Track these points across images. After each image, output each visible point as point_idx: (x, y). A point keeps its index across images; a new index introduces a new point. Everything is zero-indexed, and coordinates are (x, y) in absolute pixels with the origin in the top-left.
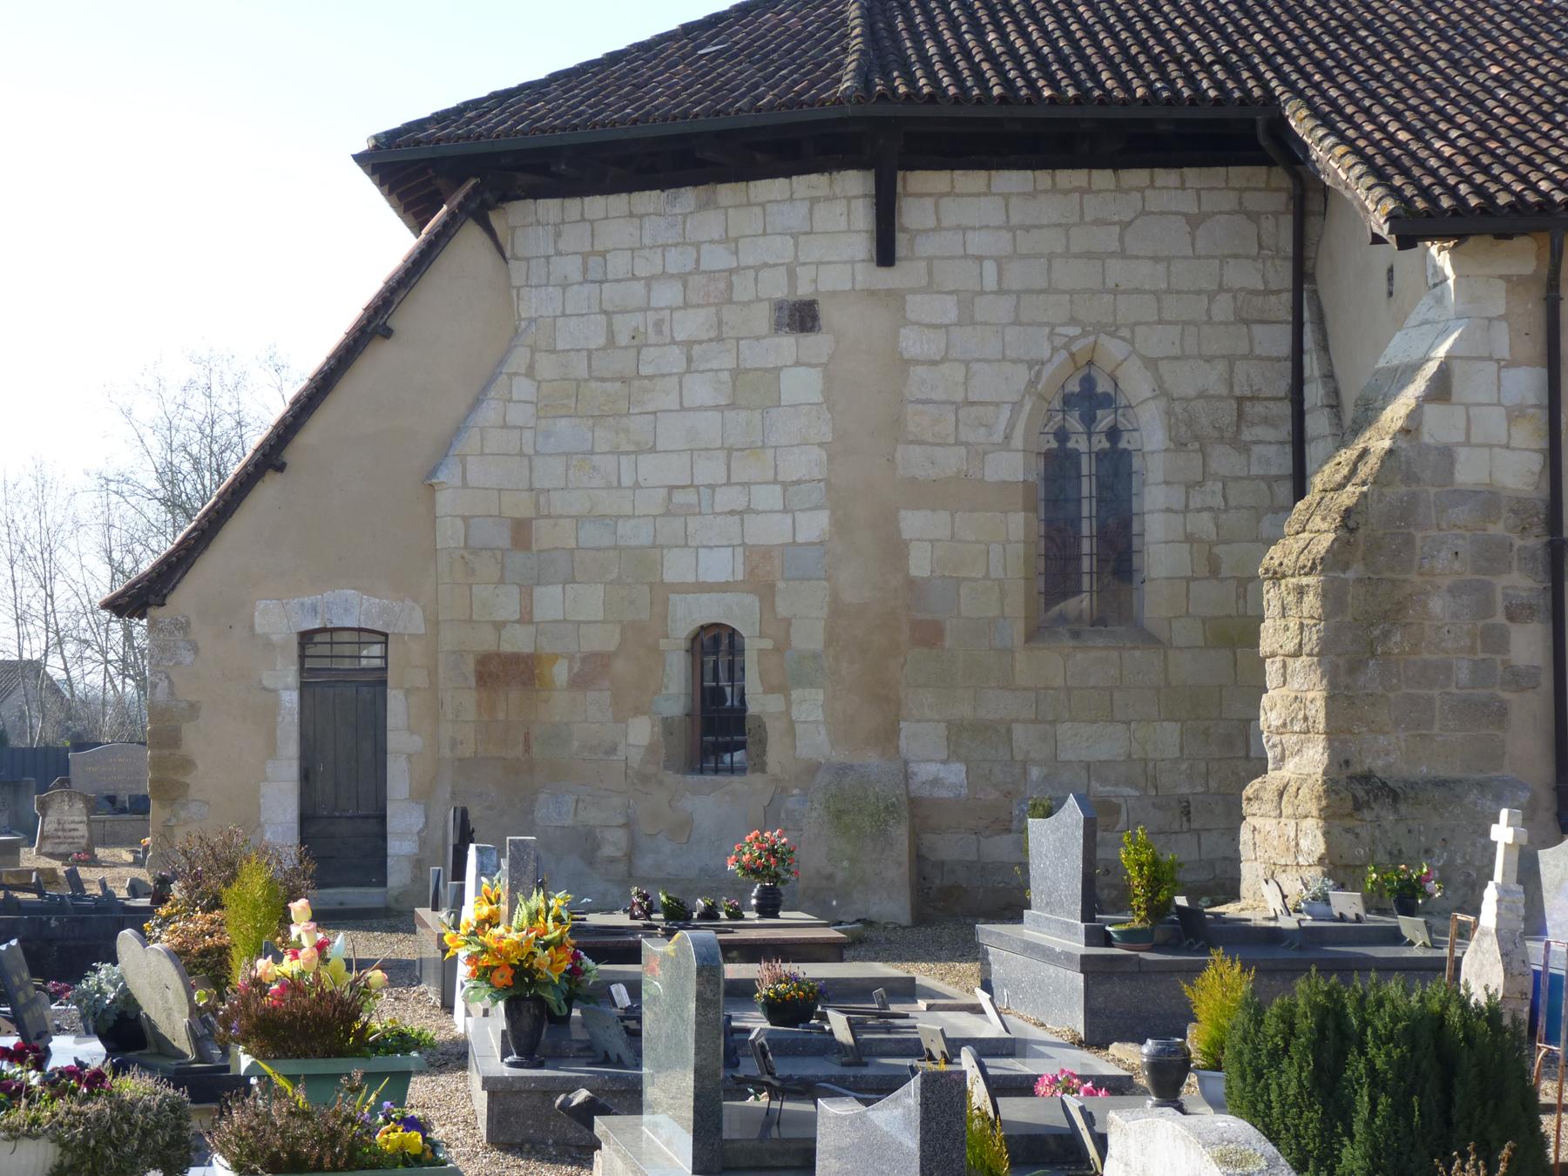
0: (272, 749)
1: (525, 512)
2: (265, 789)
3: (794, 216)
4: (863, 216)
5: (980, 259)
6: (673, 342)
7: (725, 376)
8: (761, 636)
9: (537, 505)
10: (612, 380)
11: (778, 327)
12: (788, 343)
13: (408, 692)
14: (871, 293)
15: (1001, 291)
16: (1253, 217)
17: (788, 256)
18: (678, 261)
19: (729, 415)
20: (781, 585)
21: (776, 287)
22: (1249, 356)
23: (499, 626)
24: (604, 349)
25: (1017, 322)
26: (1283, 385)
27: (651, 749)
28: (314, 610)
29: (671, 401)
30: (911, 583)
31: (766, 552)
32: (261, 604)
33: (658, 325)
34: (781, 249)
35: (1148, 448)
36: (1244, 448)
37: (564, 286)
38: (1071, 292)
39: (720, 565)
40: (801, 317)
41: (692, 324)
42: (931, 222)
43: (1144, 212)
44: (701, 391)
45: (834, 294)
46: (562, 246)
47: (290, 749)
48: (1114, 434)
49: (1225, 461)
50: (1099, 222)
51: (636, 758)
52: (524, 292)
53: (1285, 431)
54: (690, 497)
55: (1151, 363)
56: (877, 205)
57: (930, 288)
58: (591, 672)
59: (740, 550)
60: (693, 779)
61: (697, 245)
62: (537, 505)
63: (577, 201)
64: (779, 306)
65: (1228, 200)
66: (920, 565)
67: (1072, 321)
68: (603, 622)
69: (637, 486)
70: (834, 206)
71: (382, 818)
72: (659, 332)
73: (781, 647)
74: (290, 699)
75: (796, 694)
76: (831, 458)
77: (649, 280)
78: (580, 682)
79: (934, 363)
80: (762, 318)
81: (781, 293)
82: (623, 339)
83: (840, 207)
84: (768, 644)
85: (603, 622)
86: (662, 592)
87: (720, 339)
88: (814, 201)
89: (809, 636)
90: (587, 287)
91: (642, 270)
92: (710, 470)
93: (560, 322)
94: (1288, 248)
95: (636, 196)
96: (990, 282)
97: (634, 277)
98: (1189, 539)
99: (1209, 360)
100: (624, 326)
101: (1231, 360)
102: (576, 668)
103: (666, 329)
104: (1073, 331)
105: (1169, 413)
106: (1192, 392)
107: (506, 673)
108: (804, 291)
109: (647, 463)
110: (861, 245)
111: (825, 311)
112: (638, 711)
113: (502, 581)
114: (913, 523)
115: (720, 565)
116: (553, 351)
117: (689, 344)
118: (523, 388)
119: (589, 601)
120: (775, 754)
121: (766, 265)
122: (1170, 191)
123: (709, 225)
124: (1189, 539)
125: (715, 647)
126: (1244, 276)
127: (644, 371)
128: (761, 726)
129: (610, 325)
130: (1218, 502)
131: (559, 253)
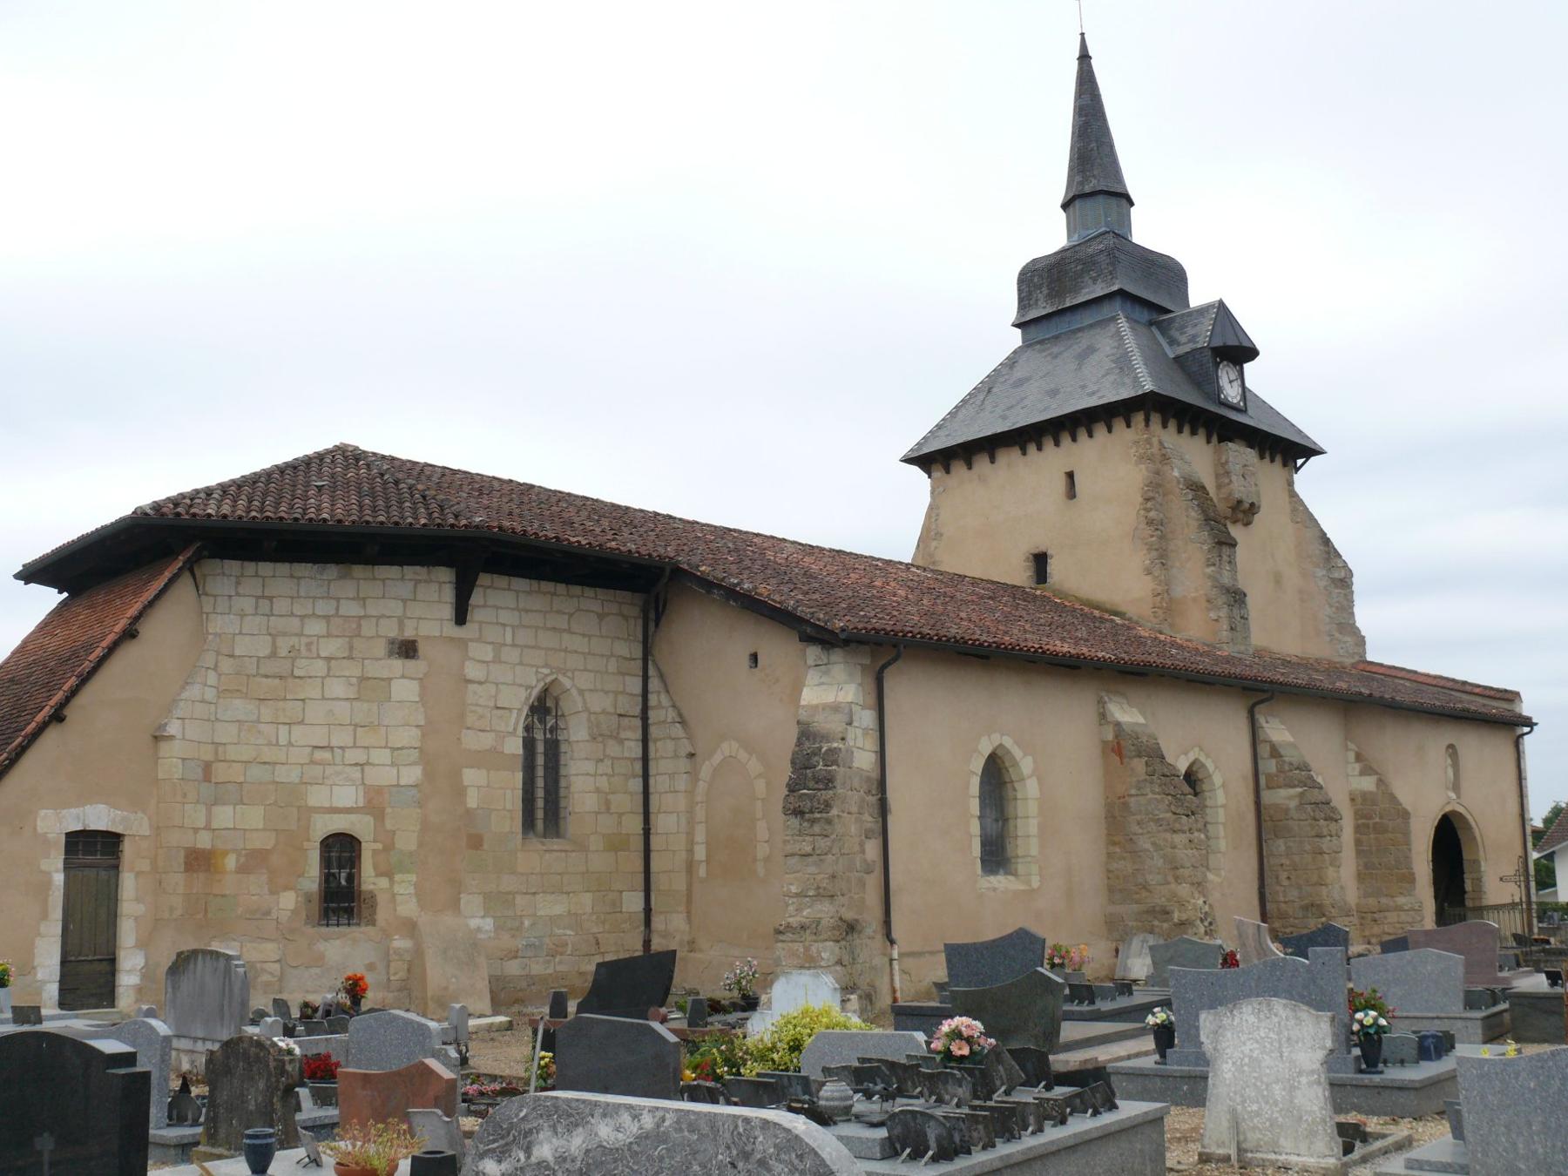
0: (45, 916)
1: (209, 757)
2: (38, 941)
3: (405, 589)
4: (449, 594)
5: (504, 625)
6: (319, 657)
7: (354, 680)
8: (375, 841)
9: (216, 753)
10: (274, 677)
11: (390, 654)
12: (398, 664)
13: (138, 874)
14: (452, 639)
15: (514, 645)
16: (626, 618)
17: (399, 612)
18: (324, 607)
19: (356, 704)
20: (389, 810)
21: (391, 630)
22: (623, 693)
23: (196, 830)
24: (269, 657)
25: (521, 663)
26: (637, 710)
27: (295, 912)
28: (78, 818)
29: (316, 693)
30: (468, 811)
31: (379, 790)
32: (42, 813)
33: (309, 645)
34: (395, 608)
35: (573, 738)
36: (621, 742)
37: (242, 615)
38: (548, 649)
39: (347, 796)
40: (407, 649)
41: (331, 647)
42: (481, 602)
43: (579, 610)
44: (337, 688)
45: (428, 637)
46: (241, 591)
47: (57, 914)
48: (554, 729)
49: (613, 749)
50: (558, 612)
51: (284, 917)
52: (212, 616)
53: (639, 734)
54: (327, 755)
55: (581, 692)
56: (457, 589)
57: (480, 640)
58: (254, 861)
59: (361, 788)
60: (324, 930)
61: (338, 600)
62: (216, 753)
63: (253, 564)
64: (392, 642)
65: (614, 608)
66: (472, 801)
67: (546, 666)
68: (264, 830)
69: (290, 744)
70: (437, 587)
71: (113, 961)
72: (309, 650)
73: (389, 848)
74: (59, 878)
75: (397, 877)
76: (423, 735)
77: (302, 617)
78: (243, 869)
79: (480, 683)
80: (380, 648)
81: (393, 634)
82: (283, 652)
83: (435, 587)
84: (379, 846)
85: (264, 830)
86: (307, 812)
87: (350, 658)
88: (417, 582)
89: (407, 841)
90: (258, 619)
91: (298, 610)
92: (341, 738)
93: (237, 638)
94: (640, 637)
95: (296, 565)
96: (509, 640)
97: (292, 615)
98: (598, 790)
99: (606, 693)
100: (283, 645)
101: (616, 693)
102: (242, 860)
103: (314, 648)
104: (546, 671)
105: (589, 720)
106: (598, 710)
107: (199, 861)
108: (409, 634)
109: (297, 731)
110: (448, 611)
111: (422, 647)
112: (286, 888)
113: (198, 802)
114: (471, 776)
115: (347, 796)
116: (232, 656)
117: (328, 659)
118: (212, 678)
119: (254, 817)
120: (382, 915)
121: (383, 616)
122: (591, 601)
123: (346, 588)
124: (598, 790)
125: (341, 851)
126: (622, 649)
127: (297, 672)
128: (373, 896)
129: (274, 643)
130: (610, 771)
131: (238, 594)
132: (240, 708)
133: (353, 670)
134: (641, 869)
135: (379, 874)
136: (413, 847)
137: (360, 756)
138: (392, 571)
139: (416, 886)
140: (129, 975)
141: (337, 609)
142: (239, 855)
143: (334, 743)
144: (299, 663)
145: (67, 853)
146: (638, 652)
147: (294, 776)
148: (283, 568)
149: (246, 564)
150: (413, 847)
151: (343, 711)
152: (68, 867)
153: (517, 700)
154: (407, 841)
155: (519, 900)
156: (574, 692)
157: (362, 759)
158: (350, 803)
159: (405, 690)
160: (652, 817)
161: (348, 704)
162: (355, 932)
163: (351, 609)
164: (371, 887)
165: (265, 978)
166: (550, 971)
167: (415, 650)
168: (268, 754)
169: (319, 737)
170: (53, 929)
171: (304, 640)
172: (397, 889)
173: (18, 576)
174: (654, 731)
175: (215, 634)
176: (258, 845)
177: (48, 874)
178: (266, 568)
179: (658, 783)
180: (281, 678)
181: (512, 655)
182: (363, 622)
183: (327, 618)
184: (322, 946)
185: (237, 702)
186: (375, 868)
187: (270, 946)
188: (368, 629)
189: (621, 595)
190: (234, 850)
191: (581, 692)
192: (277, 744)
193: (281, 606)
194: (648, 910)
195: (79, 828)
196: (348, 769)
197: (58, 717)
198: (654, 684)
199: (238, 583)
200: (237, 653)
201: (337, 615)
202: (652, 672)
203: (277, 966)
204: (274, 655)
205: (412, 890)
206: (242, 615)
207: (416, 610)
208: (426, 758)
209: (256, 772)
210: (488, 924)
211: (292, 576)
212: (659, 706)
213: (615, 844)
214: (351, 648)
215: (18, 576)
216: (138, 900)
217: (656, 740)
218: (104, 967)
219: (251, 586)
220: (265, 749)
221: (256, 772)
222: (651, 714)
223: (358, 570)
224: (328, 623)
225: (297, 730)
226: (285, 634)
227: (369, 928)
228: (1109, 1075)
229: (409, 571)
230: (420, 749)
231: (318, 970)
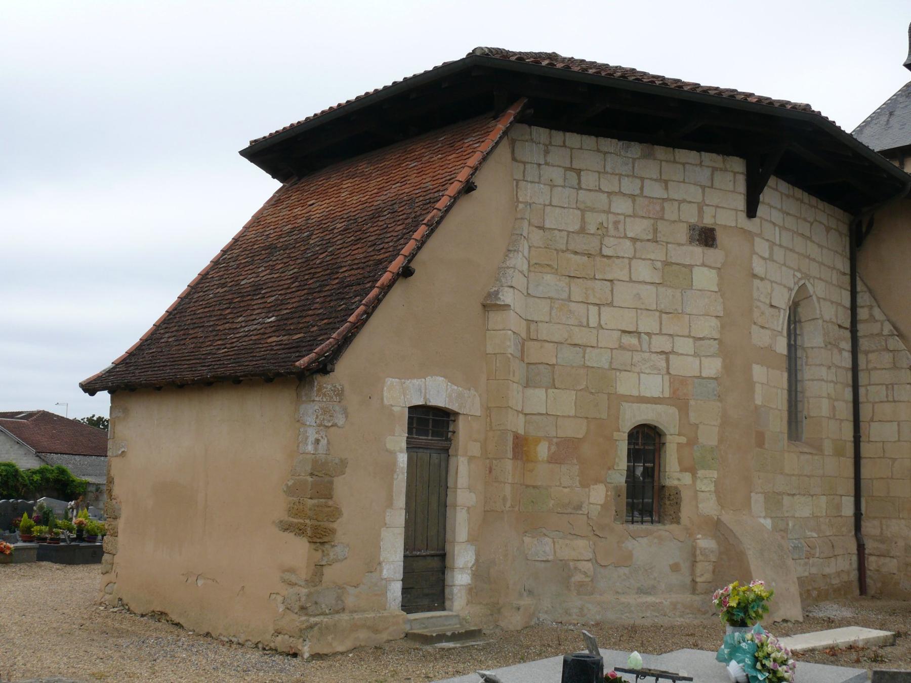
3: (703, 175)
4: (742, 187)
6: (626, 237)
10: (583, 254)
11: (691, 240)
12: (698, 251)
13: (471, 459)
18: (629, 186)
19: (661, 289)
20: (692, 402)
21: (691, 215)
29: (623, 275)
30: (757, 407)
32: (389, 381)
34: (694, 193)
35: (807, 344)
37: (552, 186)
40: (706, 237)
44: (643, 271)
46: (549, 159)
47: (401, 501)
54: (634, 341)
55: (818, 298)
58: (565, 450)
59: (667, 377)
60: (636, 527)
63: (561, 133)
64: (692, 228)
67: (799, 270)
68: (575, 417)
69: (600, 326)
72: (617, 228)
73: (693, 442)
74: (403, 459)
75: (701, 473)
76: (723, 327)
77: (610, 194)
78: (554, 459)
80: (682, 234)
81: (694, 220)
82: (592, 229)
84: (683, 440)
88: (714, 169)
89: (709, 436)
90: (567, 191)
92: (648, 324)
100: (593, 221)
102: (553, 448)
103: (621, 227)
107: (521, 447)
108: (708, 221)
110: (740, 203)
111: (720, 236)
112: (597, 481)
115: (654, 385)
116: (542, 228)
117: (634, 240)
119: (565, 402)
120: (686, 512)
121: (684, 201)
123: (649, 169)
131: (547, 164)
132: (550, 283)
133: (657, 253)
134: (852, 475)
135: (683, 470)
136: (714, 442)
137: (661, 343)
138: (690, 156)
139: (716, 483)
140: (460, 578)
141: (642, 189)
142: (550, 444)
143: (640, 330)
144: (609, 241)
145: (410, 431)
146: (843, 265)
147: (604, 362)
148: (589, 141)
149: (554, 132)
150: (714, 442)
151: (649, 294)
152: (411, 447)
153: (782, 299)
154: (709, 436)
155: (786, 500)
156: (814, 298)
157: (668, 348)
158: (656, 394)
159: (705, 278)
160: (863, 426)
161: (653, 289)
162: (663, 530)
163: (655, 190)
164: (676, 483)
165: (578, 578)
166: (806, 574)
167: (714, 239)
168: (580, 336)
169: (627, 321)
170: (397, 518)
171: (612, 218)
172: (700, 485)
173: (244, 153)
174: (864, 344)
175: (526, 203)
176: (570, 433)
177: (392, 453)
178: (573, 139)
179: (871, 393)
180: (589, 255)
181: (779, 254)
182: (666, 204)
183: (633, 197)
184: (630, 544)
185: (548, 277)
186: (680, 463)
187: (581, 543)
188: (671, 212)
189: (839, 212)
190: (548, 439)
191: (818, 298)
192: (588, 326)
193: (589, 179)
194: (858, 516)
195: (420, 402)
196: (654, 357)
197: (407, 272)
198: (863, 299)
199: (547, 152)
200: (547, 225)
201: (641, 194)
202: (860, 287)
203: (589, 565)
204: (582, 230)
205: (712, 488)
206: (552, 186)
207: (713, 198)
208: (724, 351)
209: (568, 355)
210: (768, 523)
211: (598, 151)
212: (872, 318)
213: (839, 452)
214: (655, 231)
215: (244, 153)
216: (470, 489)
217: (867, 353)
218: (435, 563)
219: (558, 156)
220: (577, 329)
221: (568, 355)
222: (862, 329)
223: (661, 152)
224: (634, 202)
225: (605, 310)
226: (592, 210)
227: (673, 527)
228: (104, 552)
229: (707, 157)
230: (720, 341)
231: (626, 570)
